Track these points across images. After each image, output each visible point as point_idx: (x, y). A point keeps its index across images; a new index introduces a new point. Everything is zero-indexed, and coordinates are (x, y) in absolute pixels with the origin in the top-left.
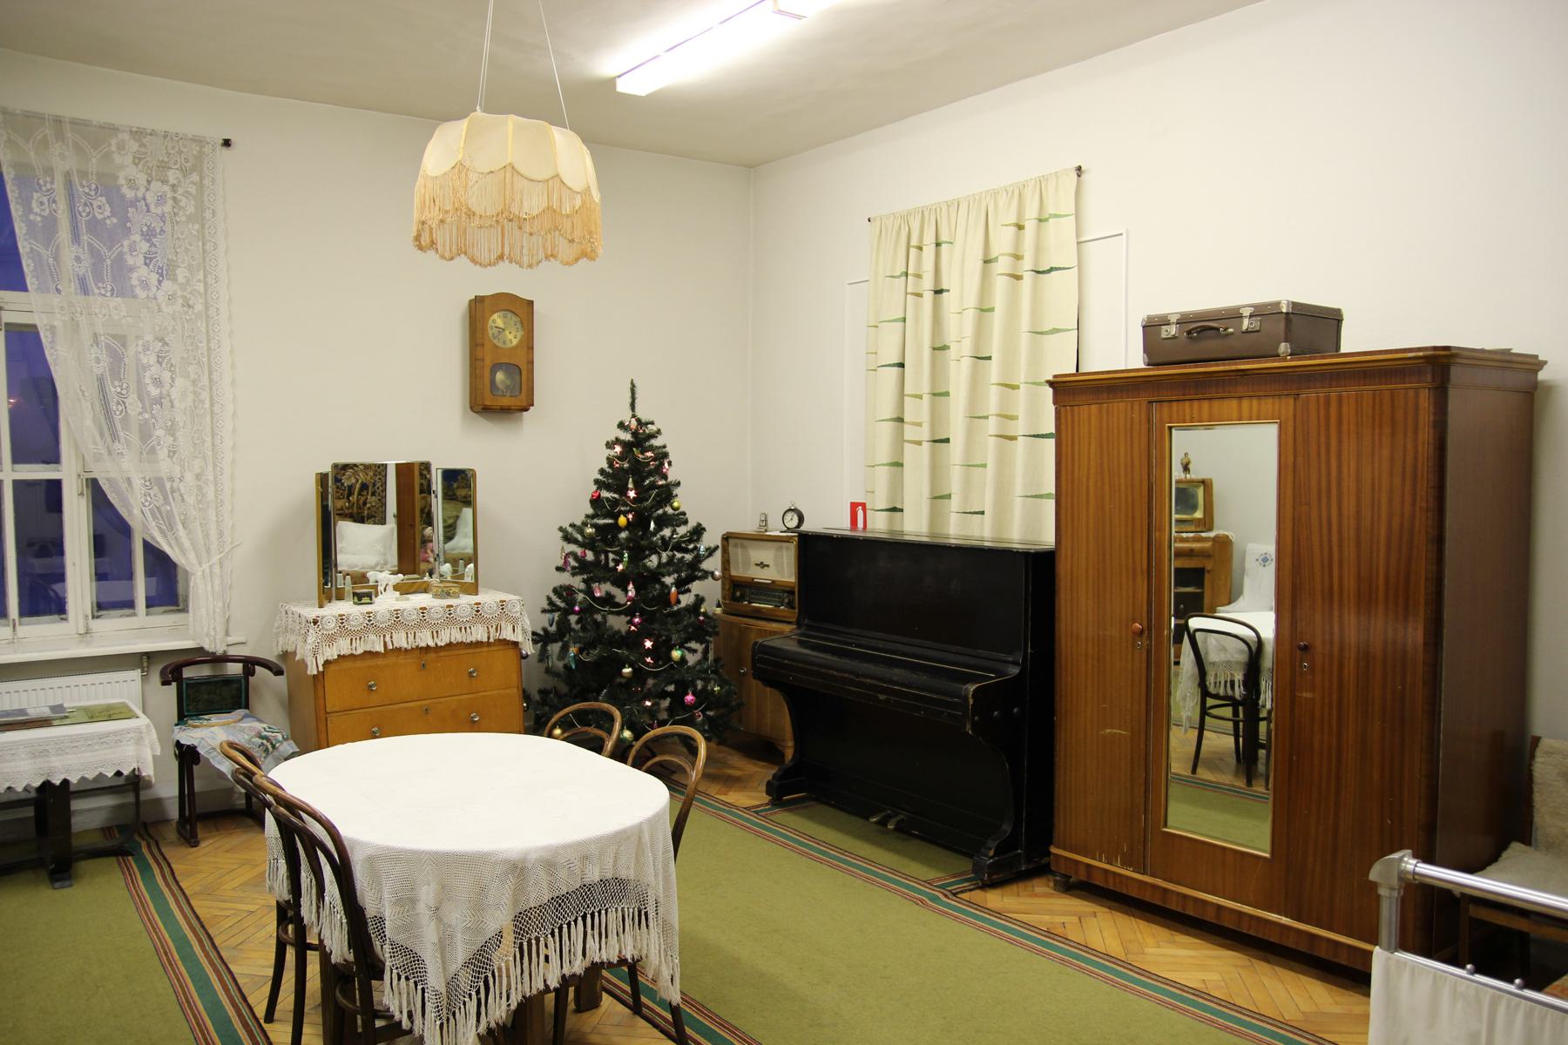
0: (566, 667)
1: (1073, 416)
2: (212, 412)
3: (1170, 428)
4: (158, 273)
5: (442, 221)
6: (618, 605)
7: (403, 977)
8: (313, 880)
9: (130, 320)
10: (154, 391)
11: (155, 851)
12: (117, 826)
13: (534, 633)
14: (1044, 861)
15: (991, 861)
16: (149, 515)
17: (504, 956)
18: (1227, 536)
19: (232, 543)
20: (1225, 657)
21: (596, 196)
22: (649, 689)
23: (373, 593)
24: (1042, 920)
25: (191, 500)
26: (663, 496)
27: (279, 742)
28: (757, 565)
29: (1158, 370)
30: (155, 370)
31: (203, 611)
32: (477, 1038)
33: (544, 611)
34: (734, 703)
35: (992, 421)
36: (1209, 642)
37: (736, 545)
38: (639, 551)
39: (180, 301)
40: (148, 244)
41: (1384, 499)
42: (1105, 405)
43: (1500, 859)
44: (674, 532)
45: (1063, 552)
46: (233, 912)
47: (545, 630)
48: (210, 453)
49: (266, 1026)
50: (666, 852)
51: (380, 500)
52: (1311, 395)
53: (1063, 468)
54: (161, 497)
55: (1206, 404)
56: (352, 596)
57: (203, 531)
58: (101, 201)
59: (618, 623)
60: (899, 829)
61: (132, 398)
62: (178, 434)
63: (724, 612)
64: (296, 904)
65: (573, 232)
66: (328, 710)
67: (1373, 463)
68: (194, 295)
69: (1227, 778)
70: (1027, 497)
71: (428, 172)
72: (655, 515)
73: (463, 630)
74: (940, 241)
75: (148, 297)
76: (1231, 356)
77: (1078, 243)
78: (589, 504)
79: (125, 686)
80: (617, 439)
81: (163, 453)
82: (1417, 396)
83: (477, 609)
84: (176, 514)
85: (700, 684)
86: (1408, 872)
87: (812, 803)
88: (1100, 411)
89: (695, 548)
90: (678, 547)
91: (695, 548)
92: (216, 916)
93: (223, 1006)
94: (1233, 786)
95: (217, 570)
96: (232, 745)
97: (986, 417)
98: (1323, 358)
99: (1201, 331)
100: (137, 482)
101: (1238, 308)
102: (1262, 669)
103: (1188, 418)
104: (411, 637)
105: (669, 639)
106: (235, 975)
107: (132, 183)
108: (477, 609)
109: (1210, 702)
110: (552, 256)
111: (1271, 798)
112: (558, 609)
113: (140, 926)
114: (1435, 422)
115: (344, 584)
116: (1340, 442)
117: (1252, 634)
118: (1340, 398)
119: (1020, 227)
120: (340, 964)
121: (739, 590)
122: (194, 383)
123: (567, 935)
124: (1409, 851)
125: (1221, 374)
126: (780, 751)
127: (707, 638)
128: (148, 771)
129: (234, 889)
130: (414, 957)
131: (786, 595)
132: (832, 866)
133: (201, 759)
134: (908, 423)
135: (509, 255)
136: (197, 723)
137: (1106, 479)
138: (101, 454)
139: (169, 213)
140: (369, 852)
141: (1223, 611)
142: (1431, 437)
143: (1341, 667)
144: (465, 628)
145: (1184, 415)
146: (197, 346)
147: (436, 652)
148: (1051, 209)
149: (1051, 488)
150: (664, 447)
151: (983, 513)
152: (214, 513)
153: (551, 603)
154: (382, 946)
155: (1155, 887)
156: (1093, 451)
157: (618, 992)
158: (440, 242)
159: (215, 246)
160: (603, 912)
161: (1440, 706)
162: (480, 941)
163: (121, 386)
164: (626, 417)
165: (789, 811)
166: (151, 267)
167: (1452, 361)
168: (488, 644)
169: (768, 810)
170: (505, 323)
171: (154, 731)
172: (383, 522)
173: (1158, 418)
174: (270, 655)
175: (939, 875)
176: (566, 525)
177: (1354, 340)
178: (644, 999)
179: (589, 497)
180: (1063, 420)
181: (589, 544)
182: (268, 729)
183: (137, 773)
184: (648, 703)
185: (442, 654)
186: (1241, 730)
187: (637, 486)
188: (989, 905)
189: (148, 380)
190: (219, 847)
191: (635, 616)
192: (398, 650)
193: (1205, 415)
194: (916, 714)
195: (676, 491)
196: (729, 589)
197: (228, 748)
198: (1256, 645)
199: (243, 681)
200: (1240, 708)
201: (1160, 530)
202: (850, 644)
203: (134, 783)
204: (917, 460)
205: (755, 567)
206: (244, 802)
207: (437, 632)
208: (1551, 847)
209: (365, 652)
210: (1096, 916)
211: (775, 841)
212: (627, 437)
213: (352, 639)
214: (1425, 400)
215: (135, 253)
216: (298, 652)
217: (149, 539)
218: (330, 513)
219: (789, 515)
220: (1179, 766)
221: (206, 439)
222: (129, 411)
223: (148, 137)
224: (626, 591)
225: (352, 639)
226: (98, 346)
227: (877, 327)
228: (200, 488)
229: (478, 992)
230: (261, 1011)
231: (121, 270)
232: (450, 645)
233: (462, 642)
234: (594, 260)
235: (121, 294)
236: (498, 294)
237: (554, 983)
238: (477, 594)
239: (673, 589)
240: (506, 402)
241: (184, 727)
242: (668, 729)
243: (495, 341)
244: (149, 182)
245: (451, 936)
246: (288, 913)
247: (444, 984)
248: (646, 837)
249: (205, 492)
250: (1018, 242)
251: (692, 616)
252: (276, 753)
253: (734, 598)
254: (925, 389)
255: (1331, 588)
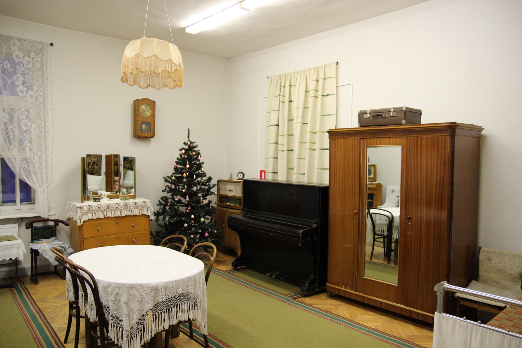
0: (165, 224)
1: (335, 143)
2: (45, 136)
3: (367, 147)
4: (27, 88)
5: (132, 73)
6: (183, 203)
7: (115, 326)
8: (84, 294)
9: (16, 104)
10: (25, 128)
11: (23, 286)
12: (9, 278)
13: (154, 213)
14: (324, 288)
15: (307, 288)
16: (22, 171)
17: (149, 319)
18: (381, 183)
19: (51, 180)
20: (381, 222)
21: (182, 67)
22: (193, 231)
23: (100, 198)
24: (324, 307)
25: (37, 166)
26: (198, 167)
27: (67, 248)
28: (229, 190)
29: (363, 128)
30: (25, 121)
31: (41, 203)
32: (140, 346)
33: (158, 205)
34: (221, 236)
35: (308, 144)
36: (376, 217)
37: (222, 184)
38: (190, 184)
39: (34, 98)
40: (23, 78)
41: (435, 170)
42: (346, 139)
43: (469, 286)
44: (202, 179)
45: (331, 187)
46: (51, 306)
47: (158, 211)
48: (44, 150)
49: (65, 345)
50: (203, 284)
51: (99, 167)
52: (412, 137)
53: (332, 159)
54: (27, 165)
55: (378, 140)
56: (92, 199)
57: (41, 176)
58: (6, 63)
59: (182, 209)
60: (275, 278)
61: (17, 131)
62: (33, 143)
63: (218, 206)
64: (77, 303)
65: (175, 78)
66: (84, 238)
67: (431, 159)
68: (39, 96)
69: (381, 261)
70: (319, 169)
71: (127, 56)
72: (195, 173)
73: (131, 211)
74: (291, 85)
75: (23, 96)
76: (387, 124)
77: (337, 87)
78: (173, 169)
79: (13, 229)
80: (183, 148)
81: (27, 150)
82: (445, 138)
83: (136, 204)
84: (32, 170)
85: (210, 230)
86: (446, 288)
87: (247, 269)
88: (344, 142)
89: (209, 184)
90: (203, 184)
91: (209, 184)
92: (45, 308)
93: (49, 338)
94: (384, 264)
95: (46, 190)
96: (55, 248)
97: (306, 143)
98: (416, 125)
99: (377, 116)
100: (18, 159)
101: (389, 109)
102: (393, 226)
103: (372, 144)
104: (113, 213)
105: (200, 214)
106: (53, 328)
107: (18, 57)
108: (136, 204)
109: (376, 237)
110: (166, 86)
111: (398, 268)
112: (162, 204)
113: (18, 312)
114: (451, 146)
115: (90, 195)
116: (421, 152)
117: (390, 214)
118: (421, 138)
119: (318, 81)
120: (93, 322)
121: (223, 199)
122: (39, 126)
123: (171, 311)
124: (446, 281)
125: (385, 130)
126: (236, 252)
127: (212, 214)
128: (21, 258)
129: (51, 299)
130: (119, 319)
131: (238, 200)
132: (254, 290)
133: (40, 254)
134: (280, 144)
135: (152, 85)
136: (38, 242)
137: (346, 163)
138: (5, 149)
139: (31, 67)
140: (104, 284)
141: (379, 207)
142: (450, 151)
143: (421, 224)
144: (131, 210)
145: (371, 143)
146: (40, 113)
147: (121, 218)
148: (328, 76)
149: (327, 166)
150: (199, 151)
151: (304, 174)
152: (45, 170)
153: (160, 202)
154: (108, 316)
155: (360, 296)
156: (342, 154)
157: (185, 331)
158: (129, 80)
159: (47, 79)
160: (183, 304)
161: (452, 237)
162: (142, 314)
163: (13, 126)
164: (186, 140)
165: (239, 272)
166: (24, 86)
167: (456, 127)
168: (139, 216)
169: (232, 272)
170: (146, 108)
171: (23, 244)
172: (100, 175)
173: (363, 144)
174: (64, 219)
175: (291, 293)
176: (165, 176)
177: (426, 120)
178: (194, 334)
179: (174, 167)
180: (332, 144)
181: (173, 183)
182: (63, 244)
183: (17, 259)
184: (192, 236)
185: (123, 219)
186: (386, 246)
187: (190, 164)
188: (307, 302)
189: (22, 124)
190: (45, 285)
191: (189, 207)
192: (108, 218)
193: (378, 143)
194: (283, 240)
195: (203, 165)
196: (219, 199)
197: (54, 249)
198: (391, 218)
199: (54, 228)
200: (386, 239)
201: (363, 180)
202: (260, 217)
203: (16, 262)
204: (283, 157)
205: (228, 191)
206: (54, 269)
207: (122, 211)
208: (484, 282)
209: (97, 218)
210: (341, 306)
211: (236, 282)
212: (186, 147)
213: (93, 214)
214: (448, 139)
215: (18, 81)
216: (74, 218)
217: (22, 179)
218: (85, 171)
219: (240, 174)
220: (367, 258)
221: (43, 145)
222: (16, 135)
223: (24, 41)
224: (186, 199)
225: (93, 214)
226: (5, 112)
227: (269, 112)
228: (40, 162)
229: (141, 331)
230: (63, 339)
231: (13, 87)
232: (126, 216)
233: (130, 215)
234: (181, 88)
235: (13, 95)
236: (143, 99)
237: (167, 328)
238: (135, 199)
239: (202, 198)
240: (146, 135)
241: (33, 243)
242: (200, 244)
243: (142, 114)
244: (24, 57)
245: (132, 312)
246: (74, 306)
247: (129, 328)
248: (197, 278)
249: (42, 163)
250: (317, 86)
251: (208, 207)
252: (66, 252)
253: (221, 202)
254: (286, 133)
255: (418, 199)
